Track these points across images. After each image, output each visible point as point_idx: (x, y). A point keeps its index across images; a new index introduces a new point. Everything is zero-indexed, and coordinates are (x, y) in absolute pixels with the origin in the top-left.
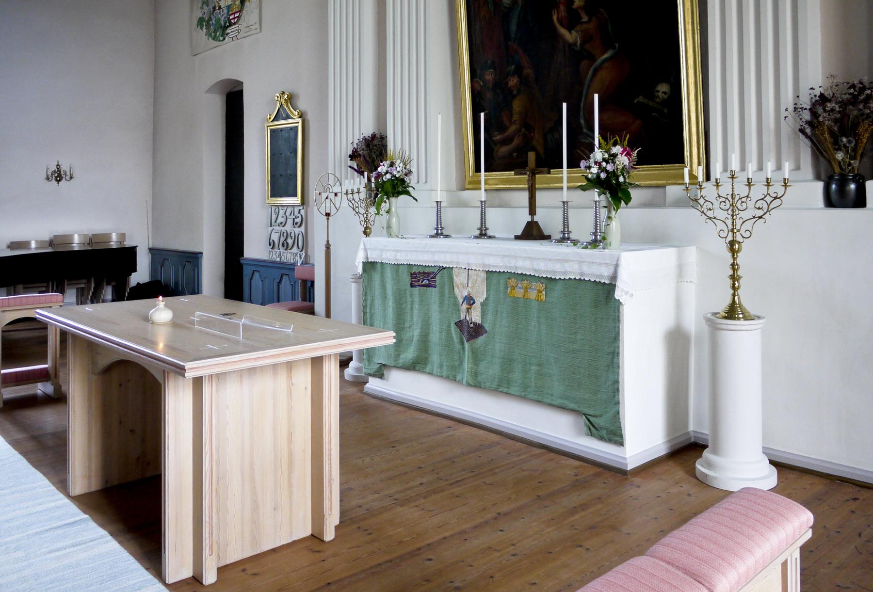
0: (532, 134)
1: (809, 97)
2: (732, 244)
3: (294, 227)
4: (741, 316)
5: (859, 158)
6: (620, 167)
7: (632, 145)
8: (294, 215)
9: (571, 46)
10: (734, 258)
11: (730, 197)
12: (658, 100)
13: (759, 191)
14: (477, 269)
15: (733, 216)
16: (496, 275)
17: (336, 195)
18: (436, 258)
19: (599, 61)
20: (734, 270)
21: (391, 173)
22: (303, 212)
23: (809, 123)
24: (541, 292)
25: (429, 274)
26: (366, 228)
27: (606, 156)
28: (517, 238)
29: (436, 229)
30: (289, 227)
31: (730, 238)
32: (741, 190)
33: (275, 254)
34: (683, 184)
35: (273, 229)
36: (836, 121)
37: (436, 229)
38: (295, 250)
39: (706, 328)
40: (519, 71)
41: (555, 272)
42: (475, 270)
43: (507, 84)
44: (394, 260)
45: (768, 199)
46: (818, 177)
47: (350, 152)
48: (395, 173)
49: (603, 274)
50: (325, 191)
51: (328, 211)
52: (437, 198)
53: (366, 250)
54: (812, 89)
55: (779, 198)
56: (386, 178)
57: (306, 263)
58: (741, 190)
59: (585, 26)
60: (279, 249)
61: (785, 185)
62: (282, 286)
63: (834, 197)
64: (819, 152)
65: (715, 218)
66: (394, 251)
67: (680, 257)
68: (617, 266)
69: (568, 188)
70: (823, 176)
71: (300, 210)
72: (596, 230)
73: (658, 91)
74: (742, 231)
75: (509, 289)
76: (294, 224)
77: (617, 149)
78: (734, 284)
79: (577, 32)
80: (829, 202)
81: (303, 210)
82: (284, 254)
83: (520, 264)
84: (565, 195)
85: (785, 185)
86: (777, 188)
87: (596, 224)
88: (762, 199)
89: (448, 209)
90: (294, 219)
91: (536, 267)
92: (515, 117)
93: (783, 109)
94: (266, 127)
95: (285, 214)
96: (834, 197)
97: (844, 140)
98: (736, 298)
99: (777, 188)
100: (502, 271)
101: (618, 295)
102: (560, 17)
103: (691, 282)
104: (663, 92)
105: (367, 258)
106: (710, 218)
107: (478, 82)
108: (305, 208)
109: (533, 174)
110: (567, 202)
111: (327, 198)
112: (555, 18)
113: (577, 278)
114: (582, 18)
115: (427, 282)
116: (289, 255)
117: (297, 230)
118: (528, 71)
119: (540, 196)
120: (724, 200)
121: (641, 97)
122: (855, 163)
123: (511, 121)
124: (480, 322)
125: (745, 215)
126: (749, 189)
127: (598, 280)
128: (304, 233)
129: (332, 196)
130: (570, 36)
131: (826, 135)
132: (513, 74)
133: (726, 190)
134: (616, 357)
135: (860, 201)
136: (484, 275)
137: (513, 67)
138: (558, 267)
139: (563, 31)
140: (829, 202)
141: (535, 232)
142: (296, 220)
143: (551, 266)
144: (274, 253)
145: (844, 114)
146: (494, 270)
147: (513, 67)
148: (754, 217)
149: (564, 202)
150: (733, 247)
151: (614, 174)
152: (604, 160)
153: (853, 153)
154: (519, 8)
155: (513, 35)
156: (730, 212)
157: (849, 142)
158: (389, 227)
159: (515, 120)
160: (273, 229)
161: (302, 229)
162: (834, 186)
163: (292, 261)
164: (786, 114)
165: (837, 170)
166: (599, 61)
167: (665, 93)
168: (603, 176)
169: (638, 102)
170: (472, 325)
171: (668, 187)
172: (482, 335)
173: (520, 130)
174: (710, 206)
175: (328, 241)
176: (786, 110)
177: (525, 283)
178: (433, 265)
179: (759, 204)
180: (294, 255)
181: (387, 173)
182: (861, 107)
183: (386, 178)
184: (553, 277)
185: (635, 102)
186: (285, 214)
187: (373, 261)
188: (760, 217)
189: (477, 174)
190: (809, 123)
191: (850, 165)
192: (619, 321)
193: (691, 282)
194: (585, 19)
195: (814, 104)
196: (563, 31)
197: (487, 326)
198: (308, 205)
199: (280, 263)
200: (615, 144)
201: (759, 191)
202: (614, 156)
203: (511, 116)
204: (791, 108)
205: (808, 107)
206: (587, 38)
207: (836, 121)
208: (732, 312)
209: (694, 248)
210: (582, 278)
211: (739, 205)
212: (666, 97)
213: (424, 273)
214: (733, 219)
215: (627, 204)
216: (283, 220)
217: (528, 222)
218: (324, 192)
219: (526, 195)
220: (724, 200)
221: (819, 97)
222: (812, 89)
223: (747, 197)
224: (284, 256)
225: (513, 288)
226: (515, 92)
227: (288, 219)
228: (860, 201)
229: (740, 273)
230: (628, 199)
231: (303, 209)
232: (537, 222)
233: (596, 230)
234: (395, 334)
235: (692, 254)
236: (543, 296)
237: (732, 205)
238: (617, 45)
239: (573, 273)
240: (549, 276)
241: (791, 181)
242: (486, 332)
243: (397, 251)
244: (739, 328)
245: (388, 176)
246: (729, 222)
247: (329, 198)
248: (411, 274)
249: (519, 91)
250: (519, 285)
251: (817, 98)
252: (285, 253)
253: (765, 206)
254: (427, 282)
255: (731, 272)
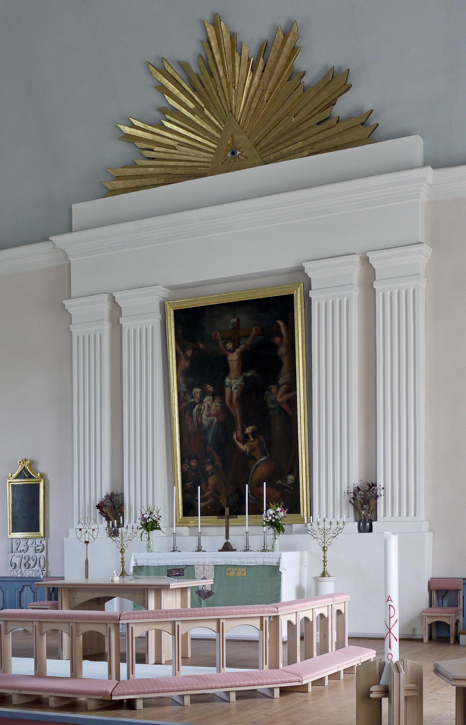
0: (220, 497)
1: (353, 488)
2: (324, 548)
3: (36, 552)
4: (327, 576)
5: (370, 513)
6: (280, 517)
7: (284, 507)
8: (35, 544)
9: (244, 452)
10: (324, 553)
11: (323, 529)
12: (288, 483)
13: (334, 526)
14: (209, 565)
15: (324, 536)
16: (219, 566)
17: (94, 530)
18: (184, 561)
19: (259, 462)
20: (324, 558)
21: (151, 518)
22: (44, 542)
23: (353, 498)
24: (244, 572)
25: (179, 569)
26: (122, 549)
27: (274, 512)
28: (220, 551)
29: (173, 548)
30: (31, 552)
31: (323, 546)
32: (328, 526)
33: (17, 572)
34: (304, 523)
35: (15, 555)
36: (362, 498)
37: (173, 548)
38: (37, 568)
39: (313, 582)
40: (212, 462)
41: (251, 563)
42: (208, 565)
43: (205, 468)
44: (156, 564)
45: (338, 530)
46: (356, 521)
47: (98, 502)
48: (154, 518)
49: (274, 562)
50: (85, 528)
51: (87, 540)
52: (173, 531)
53: (135, 560)
54: (354, 484)
55: (342, 529)
56: (148, 521)
57: (47, 577)
58: (328, 526)
59: (251, 443)
60: (21, 568)
61: (344, 524)
62: (24, 594)
63: (361, 528)
64: (356, 509)
65: (317, 538)
66: (156, 559)
67: (301, 555)
68: (280, 558)
69: (201, 526)
70: (358, 520)
71: (41, 541)
72: (264, 544)
73: (288, 479)
74: (328, 543)
75: (227, 573)
76: (36, 551)
77: (279, 509)
78: (324, 564)
79: (247, 446)
80: (360, 531)
81: (45, 541)
82: (25, 571)
83: (233, 560)
84: (247, 528)
85: (344, 524)
86: (341, 525)
87: (264, 542)
88: (335, 530)
89: (423, 522)
90: (36, 547)
91: (241, 561)
92: (210, 487)
93: (343, 493)
94: (8, 483)
95: (27, 544)
96: (361, 528)
97: (365, 506)
98: (325, 569)
99: (341, 525)
100: (223, 564)
101: (280, 570)
102: (238, 436)
103: (305, 566)
104: (291, 480)
105: (137, 564)
106: (315, 538)
107: (185, 465)
108: (46, 539)
109: (228, 518)
110: (248, 532)
111: (86, 532)
112: (235, 437)
113: (262, 564)
114: (250, 439)
115: (178, 574)
116: (31, 572)
117: (38, 555)
118: (218, 463)
119: (231, 529)
120: (321, 530)
121: (280, 481)
122: (369, 515)
123: (207, 489)
124: (210, 590)
125: (329, 536)
126: (331, 526)
127: (271, 565)
128: (45, 557)
129: (90, 531)
130: (244, 447)
131: (359, 504)
132: (209, 463)
133: (321, 526)
134: (279, 596)
135: (371, 530)
136: (213, 567)
137: (209, 459)
138: (253, 560)
139: (240, 445)
140: (360, 531)
141: (230, 548)
142: (37, 548)
143: (249, 560)
144: (15, 572)
145: (365, 495)
146: (219, 564)
147: (209, 459)
148: (332, 537)
149: (246, 532)
150: (324, 549)
151: (277, 520)
152: (273, 514)
153: (368, 511)
154: (214, 429)
155: (209, 442)
156: (323, 535)
157: (367, 507)
158: (149, 547)
159: (209, 489)
160: (15, 555)
161: (44, 553)
162: (361, 524)
163: (33, 576)
164: (344, 494)
165: (363, 518)
166: (259, 462)
167: (292, 480)
168: (273, 520)
169: (279, 483)
170: (206, 592)
171: (293, 525)
172: (212, 595)
173: (212, 494)
174: (315, 532)
175: (87, 559)
176: (344, 493)
177: (236, 569)
178: (182, 565)
179: (334, 532)
180: (36, 572)
181: (149, 518)
182: (371, 493)
183: (148, 521)
184: (250, 565)
185: (277, 483)
186: (27, 544)
187: (141, 565)
188: (335, 537)
189: (218, 520)
190: (353, 498)
191: (367, 516)
192: (280, 580)
193: (305, 566)
194: (252, 439)
195: (355, 491)
196: (240, 445)
197: (214, 591)
198: (48, 537)
199: (22, 577)
200: (277, 507)
201: (334, 526)
202: (278, 512)
203: (207, 486)
204: (346, 492)
205: (353, 492)
206: (252, 450)
207: (362, 498)
208: (324, 575)
209: (307, 551)
210: (264, 565)
211: (326, 532)
212: (292, 482)
213: (176, 569)
214: (324, 538)
215: (283, 532)
216: (25, 548)
217: (225, 543)
218: (84, 528)
219: (224, 529)
220: (321, 530)
221: (357, 488)
222: (354, 484)
223: (330, 529)
224: (26, 573)
225: (229, 572)
226: (210, 473)
227: (29, 547)
228: (371, 530)
229: (327, 559)
230: (283, 531)
231: (45, 540)
232: (229, 543)
233: (264, 544)
234: (213, 581)
235: (306, 554)
236: (245, 574)
237: (324, 532)
238: (268, 454)
239: (260, 563)
240: (248, 565)
241: (340, 522)
242: (214, 594)
243: (159, 559)
244: (328, 580)
245: (150, 520)
246: (323, 539)
247: (88, 532)
248: (168, 570)
249: (212, 474)
250: (232, 570)
251: (356, 488)
252: (26, 571)
253: (336, 533)
254: (178, 574)
255: (323, 559)
